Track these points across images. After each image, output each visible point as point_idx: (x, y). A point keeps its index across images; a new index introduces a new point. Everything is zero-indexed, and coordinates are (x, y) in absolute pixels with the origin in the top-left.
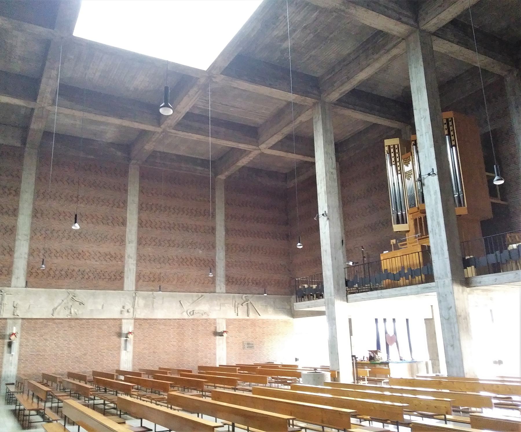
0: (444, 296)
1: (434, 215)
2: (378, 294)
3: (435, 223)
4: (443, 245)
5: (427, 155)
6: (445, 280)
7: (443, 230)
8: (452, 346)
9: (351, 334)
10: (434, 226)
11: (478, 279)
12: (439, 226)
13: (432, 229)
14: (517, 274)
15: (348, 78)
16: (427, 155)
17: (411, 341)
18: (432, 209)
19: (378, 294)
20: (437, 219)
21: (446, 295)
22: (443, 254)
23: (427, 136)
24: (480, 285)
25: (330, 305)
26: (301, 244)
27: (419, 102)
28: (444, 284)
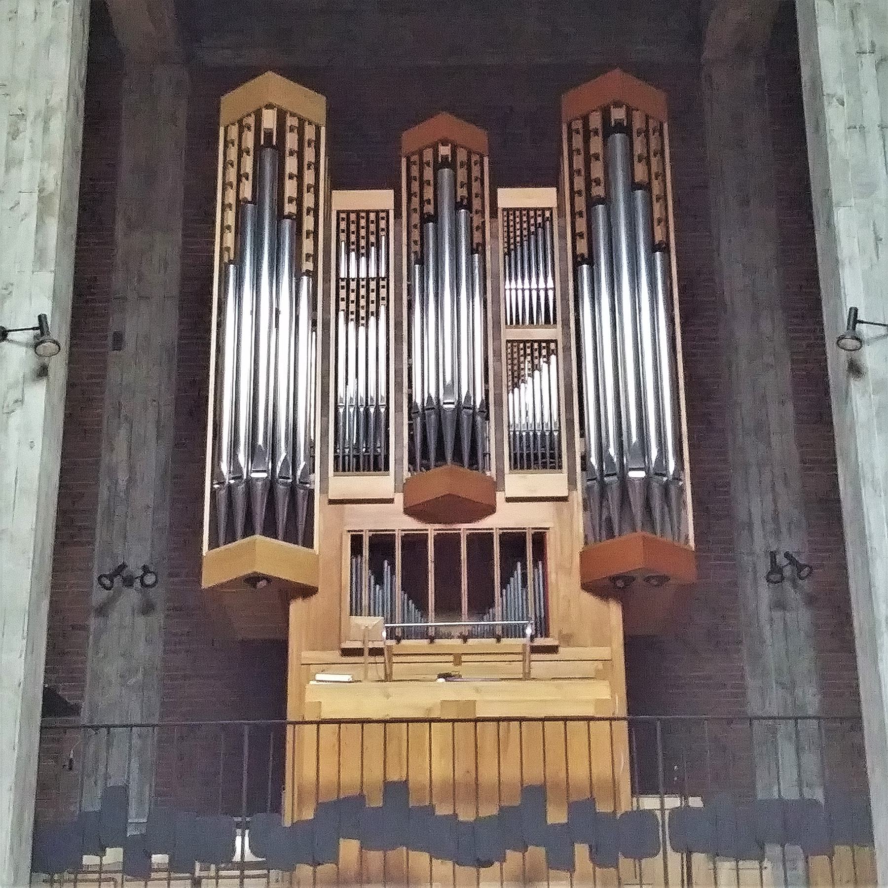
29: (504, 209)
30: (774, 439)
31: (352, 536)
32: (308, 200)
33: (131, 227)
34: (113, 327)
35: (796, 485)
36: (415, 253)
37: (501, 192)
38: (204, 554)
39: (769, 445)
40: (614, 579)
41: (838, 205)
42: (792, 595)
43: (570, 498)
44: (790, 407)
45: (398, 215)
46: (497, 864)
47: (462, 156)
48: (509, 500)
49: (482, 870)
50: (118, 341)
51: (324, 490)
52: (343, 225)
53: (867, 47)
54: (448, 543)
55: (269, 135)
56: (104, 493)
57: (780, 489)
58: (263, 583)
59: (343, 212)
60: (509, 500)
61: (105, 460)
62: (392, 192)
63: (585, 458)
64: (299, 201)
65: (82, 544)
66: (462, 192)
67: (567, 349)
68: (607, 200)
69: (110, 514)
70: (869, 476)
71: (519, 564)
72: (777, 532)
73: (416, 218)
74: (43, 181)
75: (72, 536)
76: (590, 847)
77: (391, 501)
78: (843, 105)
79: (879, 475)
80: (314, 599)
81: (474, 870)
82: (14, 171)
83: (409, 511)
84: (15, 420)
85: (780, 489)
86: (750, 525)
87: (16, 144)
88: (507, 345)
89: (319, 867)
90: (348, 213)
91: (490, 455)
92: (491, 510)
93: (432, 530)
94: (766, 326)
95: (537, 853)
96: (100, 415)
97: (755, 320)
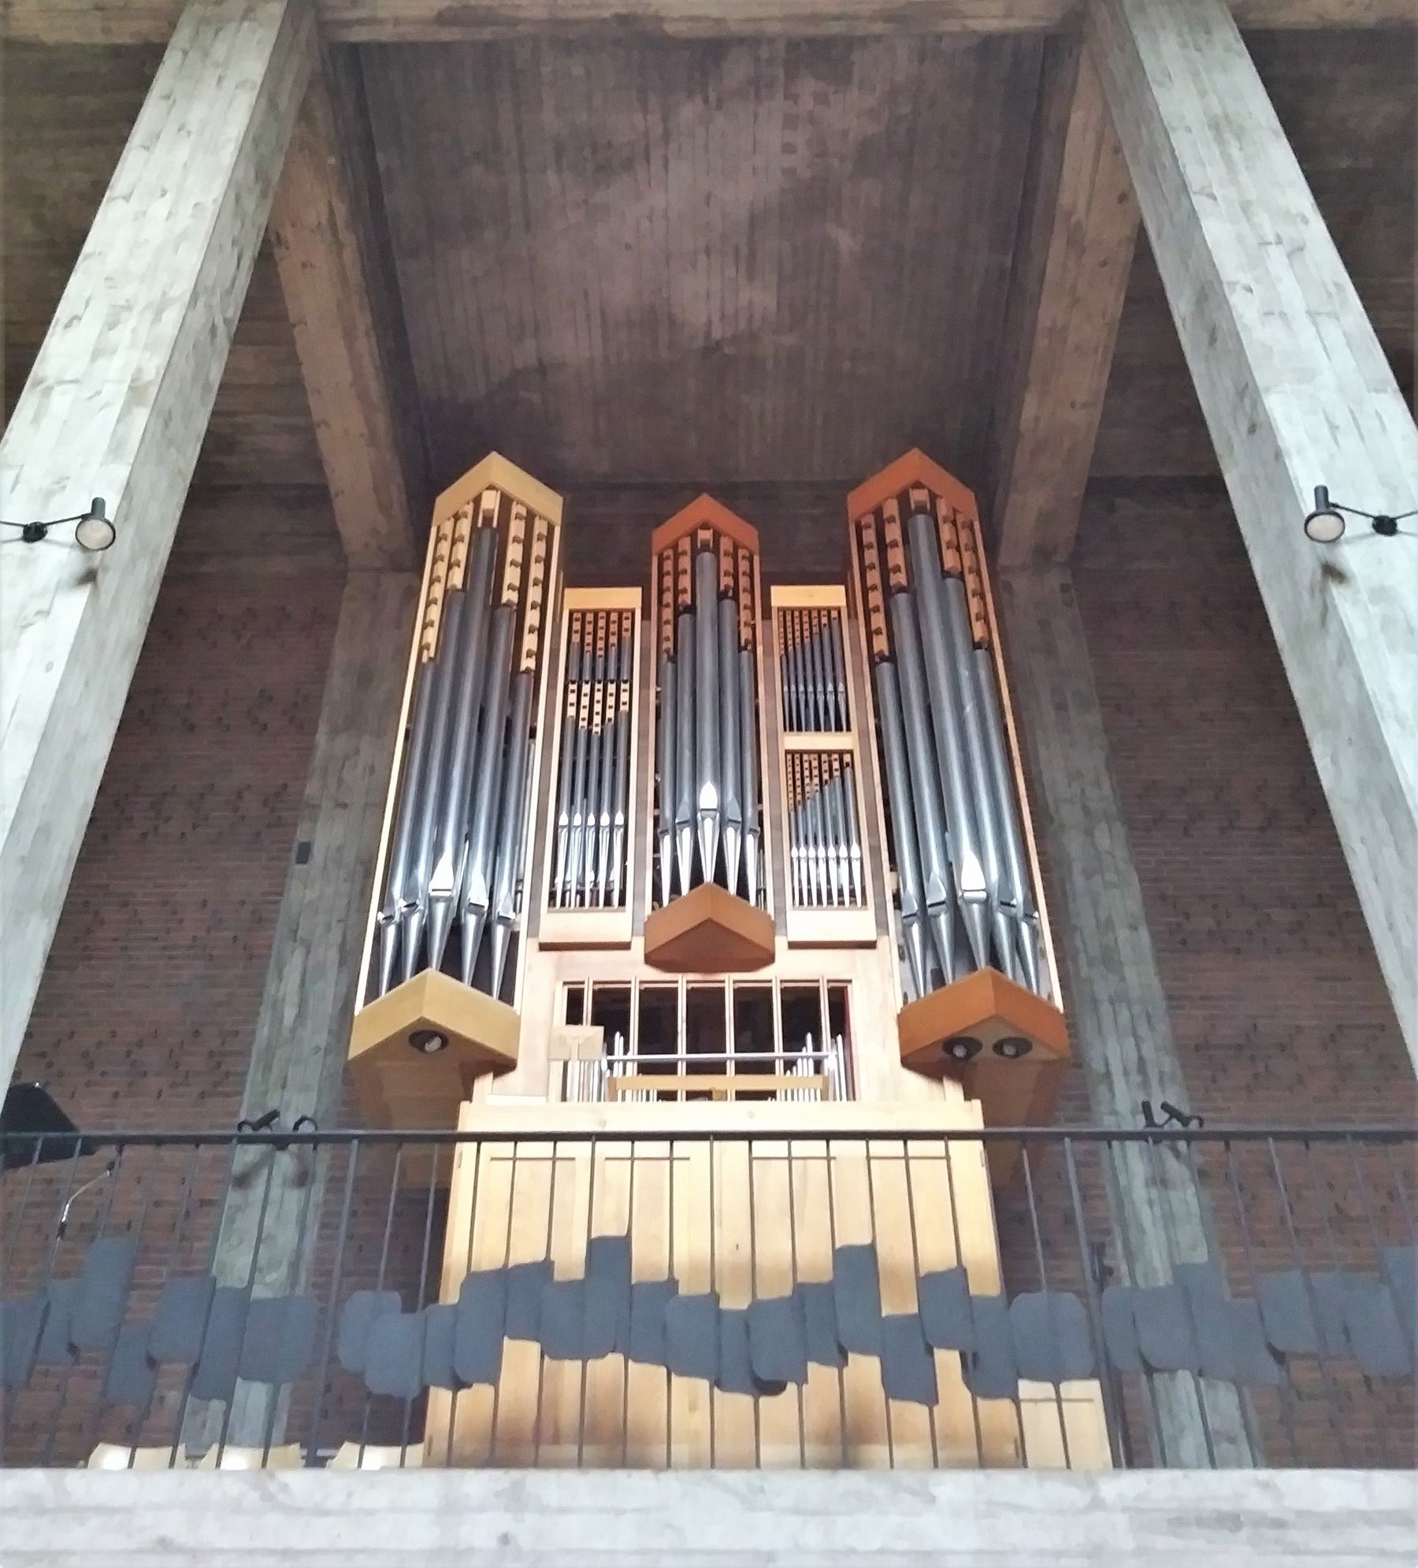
2: (450, 1509)
5: (1342, 418)
16: (1342, 418)
19: (450, 1509)
23: (1332, 331)
29: (779, 609)
30: (1130, 973)
31: (569, 990)
32: (534, 594)
33: (334, 732)
34: (301, 836)
35: (1163, 1027)
36: (667, 651)
37: (774, 589)
38: (356, 1013)
39: (1123, 979)
40: (949, 1044)
41: (1268, 390)
42: (1176, 1169)
43: (879, 945)
44: (1144, 935)
45: (646, 615)
46: (791, 1388)
47: (725, 544)
48: (793, 946)
49: (764, 1401)
50: (304, 853)
51: (533, 931)
52: (577, 626)
53: (1271, 238)
54: (705, 1004)
55: (488, 520)
56: (264, 1031)
57: (1143, 1030)
58: (434, 1044)
59: (577, 611)
60: (793, 946)
61: (271, 989)
62: (639, 590)
63: (897, 898)
64: (523, 591)
65: (228, 1095)
66: (726, 581)
67: (865, 760)
68: (912, 589)
69: (270, 1050)
70: (1388, 707)
71: (809, 1037)
72: (1145, 1084)
73: (668, 614)
74: (139, 370)
75: (216, 1084)
76: (963, 1356)
77: (626, 946)
78: (1252, 292)
79: (1406, 708)
80: (510, 1078)
81: (746, 1400)
82: (101, 362)
83: (650, 959)
84: (31, 636)
85: (1143, 1030)
86: (1108, 1075)
87: (113, 335)
88: (786, 756)
89: (462, 1394)
90: (584, 613)
91: (765, 891)
92: (769, 959)
93: (682, 983)
94: (1103, 839)
95: (865, 1369)
96: (271, 938)
97: (1089, 833)
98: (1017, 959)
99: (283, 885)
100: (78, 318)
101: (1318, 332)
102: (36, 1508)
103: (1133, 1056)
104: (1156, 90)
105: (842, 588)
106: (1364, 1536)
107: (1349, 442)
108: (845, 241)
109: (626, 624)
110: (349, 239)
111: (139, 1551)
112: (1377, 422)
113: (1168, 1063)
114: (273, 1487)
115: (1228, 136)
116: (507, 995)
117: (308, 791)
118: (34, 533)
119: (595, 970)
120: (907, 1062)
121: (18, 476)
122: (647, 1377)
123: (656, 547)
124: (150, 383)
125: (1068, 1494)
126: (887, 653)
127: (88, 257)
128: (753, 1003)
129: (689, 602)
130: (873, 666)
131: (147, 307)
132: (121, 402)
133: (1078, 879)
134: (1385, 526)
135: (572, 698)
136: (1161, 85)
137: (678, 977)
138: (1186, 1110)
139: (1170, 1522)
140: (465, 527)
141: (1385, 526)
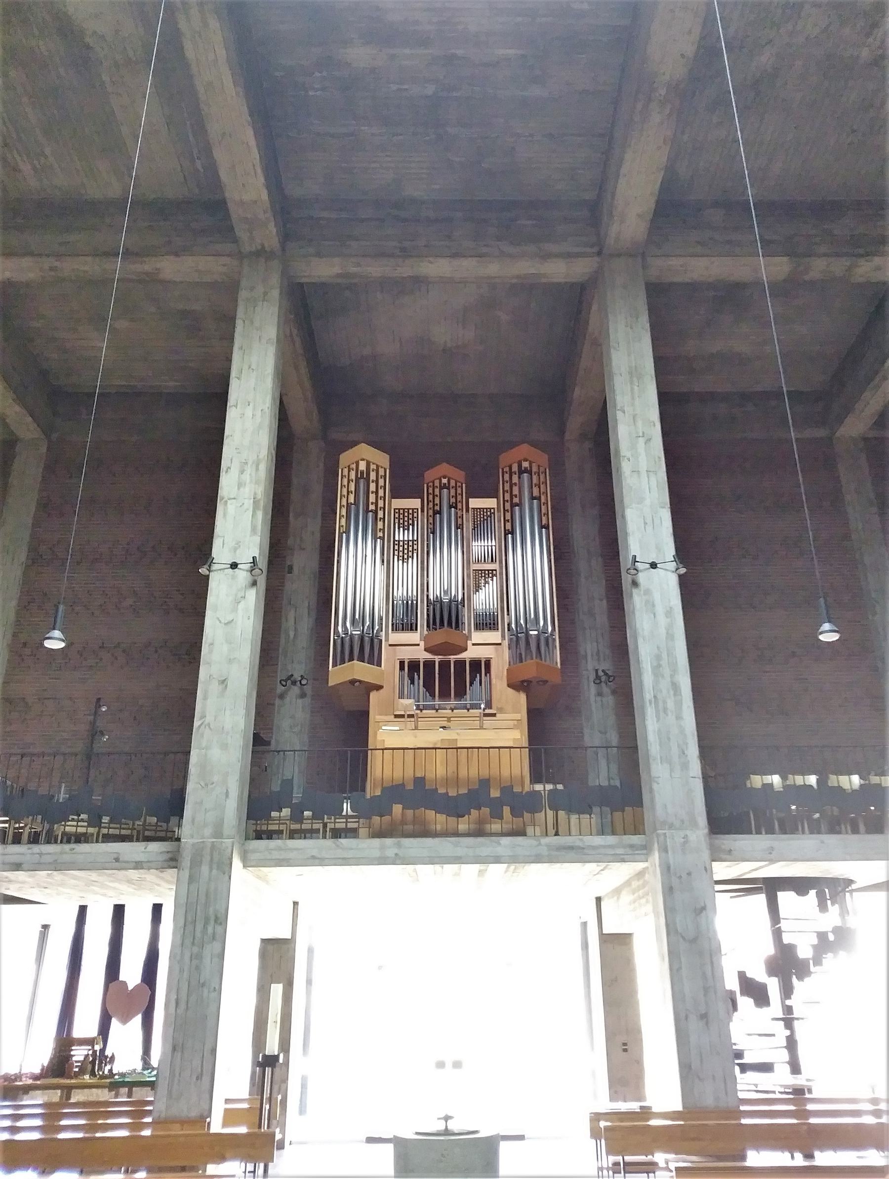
0: (684, 876)
1: (664, 663)
2: (383, 848)
3: (665, 684)
4: (687, 744)
5: (649, 521)
6: (688, 832)
7: (688, 707)
8: (704, 1017)
9: (760, 1035)
10: (661, 691)
11: (725, 842)
12: (675, 695)
13: (655, 697)
14: (822, 842)
15: (405, 253)
16: (649, 521)
17: (314, 969)
18: (658, 648)
19: (383, 848)
20: (672, 676)
21: (689, 874)
22: (685, 766)
23: (653, 480)
24: (728, 857)
25: (205, 869)
26: (61, 636)
27: (633, 398)
28: (686, 843)
40: (523, 682)
42: (606, 690)
45: (422, 511)
46: (467, 816)
47: (453, 483)
48: (474, 644)
49: (460, 819)
50: (290, 569)
51: (387, 640)
53: (641, 434)
54: (444, 665)
56: (283, 641)
60: (474, 644)
65: (273, 665)
71: (478, 675)
73: (431, 513)
77: (418, 645)
80: (381, 691)
81: (455, 819)
82: (242, 489)
87: (243, 476)
93: (437, 659)
95: (486, 811)
98: (547, 652)
99: (283, 582)
100: (229, 468)
101: (649, 480)
102: (279, 849)
103: (596, 650)
104: (612, 350)
105: (496, 499)
106: (602, 851)
107: (649, 528)
108: (504, 317)
109: (415, 515)
110: (298, 340)
111: (308, 859)
112: (659, 521)
113: (607, 652)
114: (338, 843)
115: (635, 379)
116: (379, 665)
117: (289, 542)
118: (234, 566)
119: (408, 654)
120: (509, 686)
121: (224, 540)
122: (431, 814)
123: (426, 481)
124: (260, 499)
125: (534, 842)
126: (510, 530)
127: (227, 437)
128: (460, 664)
129: (439, 509)
130: (506, 535)
131: (253, 463)
132: (251, 509)
133: (583, 580)
134: (654, 565)
135: (396, 547)
136: (615, 348)
137: (436, 657)
138: (610, 673)
139: (557, 849)
140: (353, 475)
141: (654, 565)
